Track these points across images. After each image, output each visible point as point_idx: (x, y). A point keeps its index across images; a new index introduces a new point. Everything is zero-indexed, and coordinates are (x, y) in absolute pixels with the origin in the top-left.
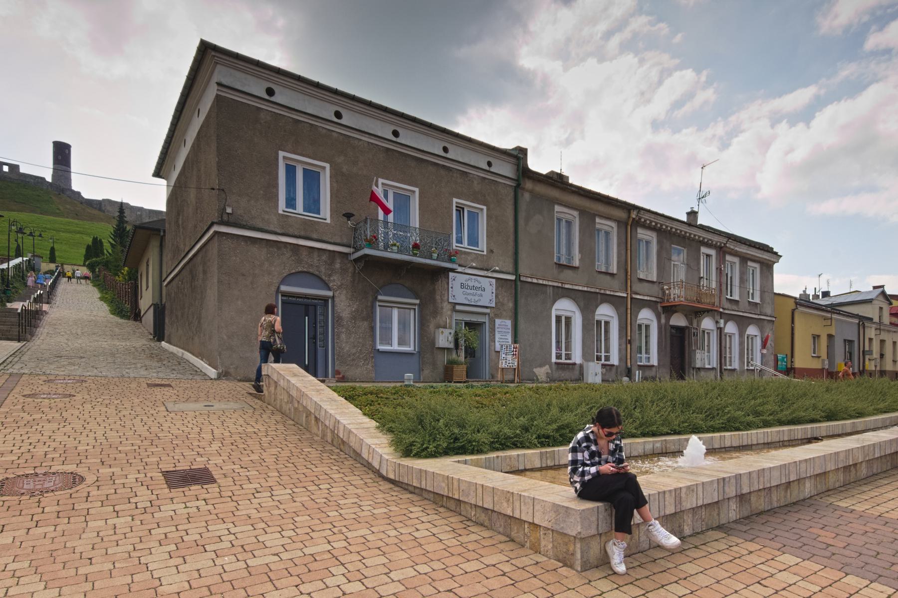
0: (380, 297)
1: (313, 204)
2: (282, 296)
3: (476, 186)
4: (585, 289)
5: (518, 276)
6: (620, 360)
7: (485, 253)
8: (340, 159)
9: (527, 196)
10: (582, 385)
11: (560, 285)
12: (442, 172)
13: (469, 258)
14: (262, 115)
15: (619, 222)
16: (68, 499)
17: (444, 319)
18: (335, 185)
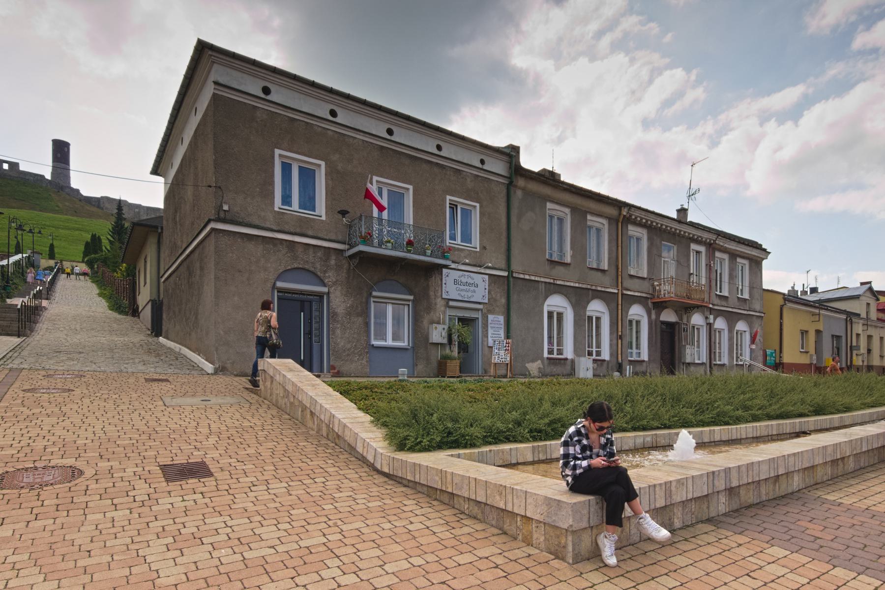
0: (374, 293)
1: (308, 202)
2: (278, 292)
3: (470, 184)
4: (577, 285)
5: (511, 272)
6: (611, 355)
7: (478, 250)
8: (335, 157)
9: (519, 193)
10: (573, 380)
11: (552, 281)
12: (436, 170)
13: (462, 255)
14: (258, 114)
15: (610, 219)
16: (67, 492)
17: (438, 315)
18: (330, 182)
